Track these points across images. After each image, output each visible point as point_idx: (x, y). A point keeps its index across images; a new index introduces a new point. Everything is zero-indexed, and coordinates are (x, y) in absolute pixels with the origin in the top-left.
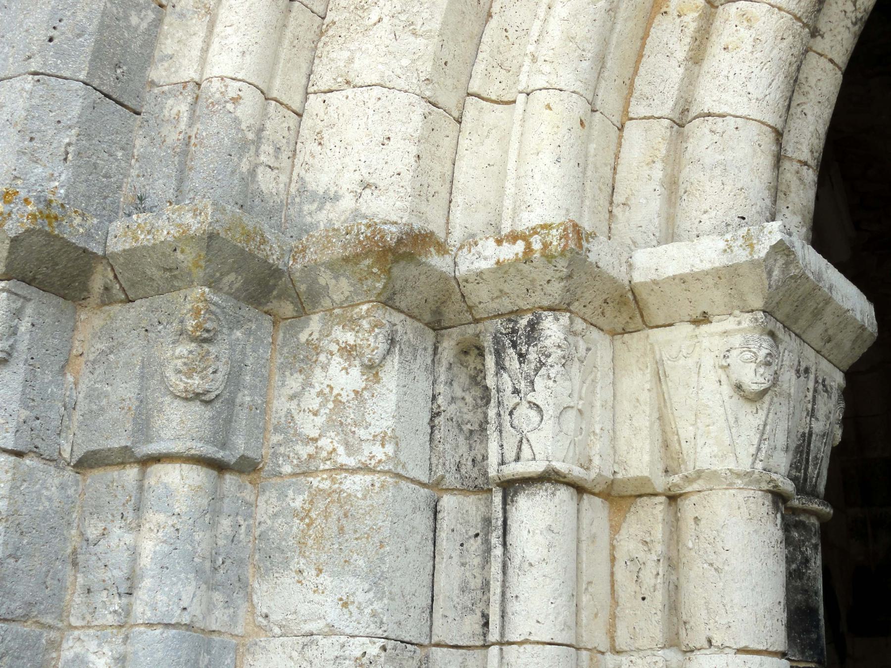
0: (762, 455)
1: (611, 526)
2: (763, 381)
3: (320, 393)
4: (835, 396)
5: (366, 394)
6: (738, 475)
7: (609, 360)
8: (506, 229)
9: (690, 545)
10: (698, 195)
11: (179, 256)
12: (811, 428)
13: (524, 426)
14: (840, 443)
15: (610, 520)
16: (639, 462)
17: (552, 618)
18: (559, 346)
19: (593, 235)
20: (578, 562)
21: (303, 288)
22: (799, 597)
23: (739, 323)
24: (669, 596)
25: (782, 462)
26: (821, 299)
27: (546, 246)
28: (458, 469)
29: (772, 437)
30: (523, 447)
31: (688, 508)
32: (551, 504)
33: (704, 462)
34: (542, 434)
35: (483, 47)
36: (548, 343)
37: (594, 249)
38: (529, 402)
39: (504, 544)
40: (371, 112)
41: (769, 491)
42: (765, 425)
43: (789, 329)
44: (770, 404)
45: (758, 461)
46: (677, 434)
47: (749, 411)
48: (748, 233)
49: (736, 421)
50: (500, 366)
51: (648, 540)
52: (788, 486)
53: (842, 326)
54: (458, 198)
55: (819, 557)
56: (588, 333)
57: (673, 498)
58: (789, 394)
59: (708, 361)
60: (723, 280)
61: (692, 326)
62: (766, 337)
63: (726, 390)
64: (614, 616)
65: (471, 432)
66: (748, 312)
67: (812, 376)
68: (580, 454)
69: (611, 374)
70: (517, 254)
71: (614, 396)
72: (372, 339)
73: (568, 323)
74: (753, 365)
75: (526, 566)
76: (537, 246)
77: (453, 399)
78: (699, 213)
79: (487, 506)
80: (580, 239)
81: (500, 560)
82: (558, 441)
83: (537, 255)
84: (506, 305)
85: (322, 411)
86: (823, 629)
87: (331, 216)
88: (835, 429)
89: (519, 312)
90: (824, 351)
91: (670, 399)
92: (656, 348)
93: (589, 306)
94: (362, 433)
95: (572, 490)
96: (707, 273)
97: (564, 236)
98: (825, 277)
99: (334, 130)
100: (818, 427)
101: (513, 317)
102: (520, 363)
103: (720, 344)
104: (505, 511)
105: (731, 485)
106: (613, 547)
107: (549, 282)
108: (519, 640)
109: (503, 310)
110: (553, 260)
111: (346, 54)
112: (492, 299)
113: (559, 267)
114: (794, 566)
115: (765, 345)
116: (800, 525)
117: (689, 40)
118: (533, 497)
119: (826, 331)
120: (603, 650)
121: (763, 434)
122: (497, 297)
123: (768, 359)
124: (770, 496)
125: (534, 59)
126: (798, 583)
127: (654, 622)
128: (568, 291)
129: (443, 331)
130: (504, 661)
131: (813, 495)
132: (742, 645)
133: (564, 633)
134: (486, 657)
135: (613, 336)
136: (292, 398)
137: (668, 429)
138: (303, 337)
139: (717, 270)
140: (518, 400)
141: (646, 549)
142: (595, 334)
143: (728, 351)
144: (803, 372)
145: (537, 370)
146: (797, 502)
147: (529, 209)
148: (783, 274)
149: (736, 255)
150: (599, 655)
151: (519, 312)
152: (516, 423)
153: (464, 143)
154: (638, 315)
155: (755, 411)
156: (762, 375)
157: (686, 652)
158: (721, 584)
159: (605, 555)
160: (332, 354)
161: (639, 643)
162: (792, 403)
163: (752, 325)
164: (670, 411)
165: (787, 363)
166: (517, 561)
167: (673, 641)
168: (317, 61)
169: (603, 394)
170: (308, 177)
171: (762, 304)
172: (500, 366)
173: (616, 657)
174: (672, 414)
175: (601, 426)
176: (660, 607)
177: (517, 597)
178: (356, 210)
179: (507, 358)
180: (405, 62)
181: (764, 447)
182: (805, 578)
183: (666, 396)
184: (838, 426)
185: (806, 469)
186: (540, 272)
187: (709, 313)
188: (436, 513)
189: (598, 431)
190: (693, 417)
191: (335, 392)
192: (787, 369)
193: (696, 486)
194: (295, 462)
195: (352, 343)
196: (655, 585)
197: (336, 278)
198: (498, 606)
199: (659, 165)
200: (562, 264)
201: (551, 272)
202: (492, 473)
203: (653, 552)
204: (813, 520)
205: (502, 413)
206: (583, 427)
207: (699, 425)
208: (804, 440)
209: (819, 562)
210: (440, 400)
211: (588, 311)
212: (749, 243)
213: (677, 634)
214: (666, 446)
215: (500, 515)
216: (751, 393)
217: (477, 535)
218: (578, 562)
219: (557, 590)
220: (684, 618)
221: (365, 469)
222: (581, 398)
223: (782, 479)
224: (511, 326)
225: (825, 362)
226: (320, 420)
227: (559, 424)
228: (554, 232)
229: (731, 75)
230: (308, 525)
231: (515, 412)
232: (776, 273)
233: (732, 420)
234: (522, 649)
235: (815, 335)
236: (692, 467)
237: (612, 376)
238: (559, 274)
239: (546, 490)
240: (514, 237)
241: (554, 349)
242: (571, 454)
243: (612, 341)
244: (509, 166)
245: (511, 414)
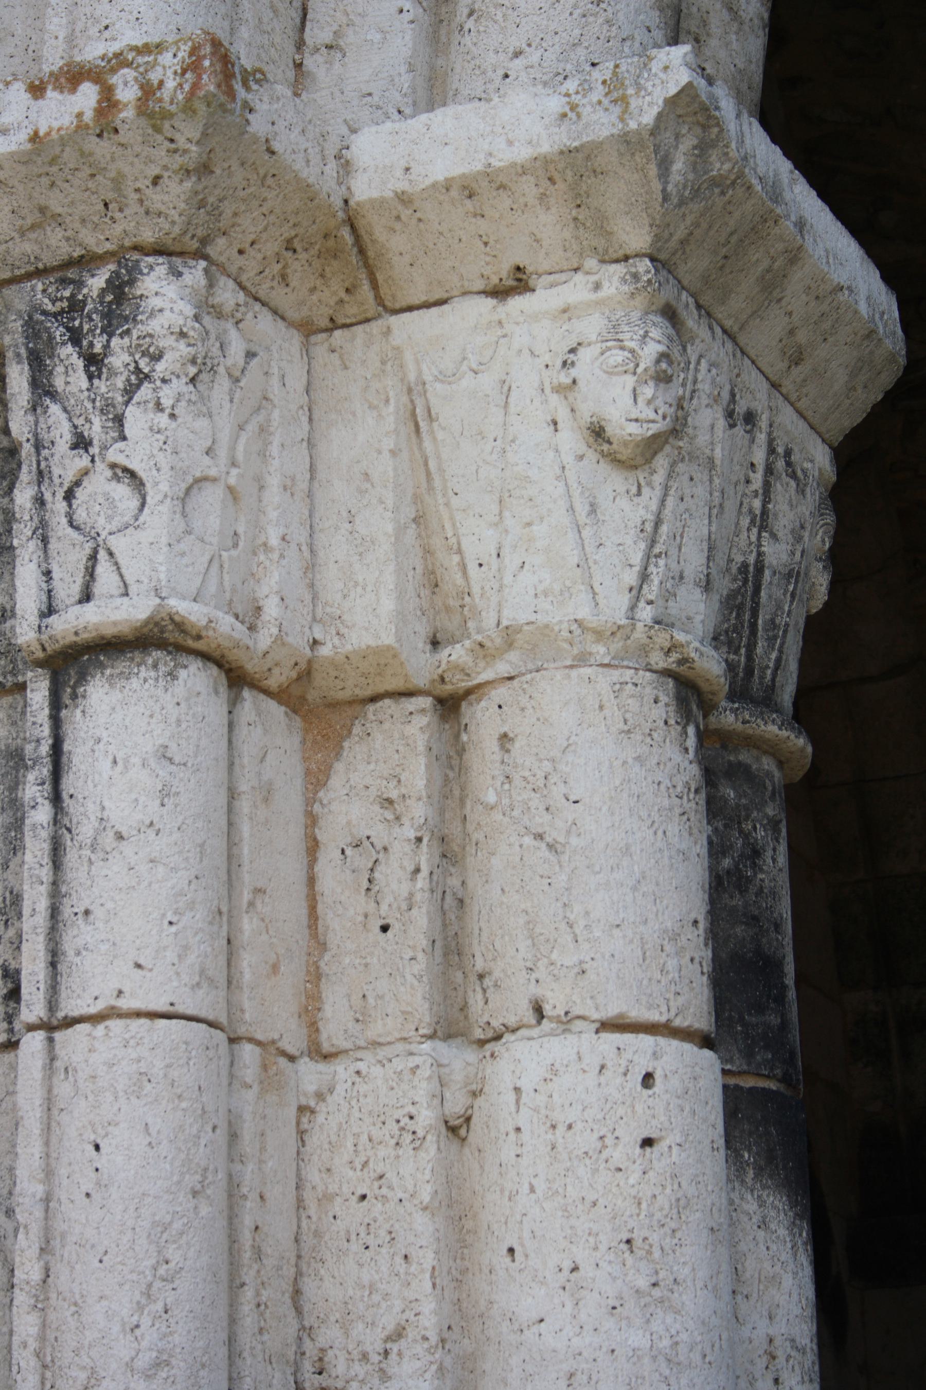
0: (652, 591)
1: (308, 772)
2: (652, 416)
4: (813, 496)
6: (599, 635)
7: (300, 385)
8: (53, 59)
9: (491, 798)
10: (499, 17)
12: (760, 554)
13: (101, 521)
14: (826, 604)
15: (305, 759)
16: (369, 615)
17: (171, 955)
18: (182, 335)
19: (255, 77)
22: (739, 930)
23: (597, 286)
24: (445, 925)
25: (697, 611)
26: (780, 246)
27: (148, 91)
29: (673, 552)
30: (99, 569)
31: (483, 719)
32: (168, 699)
33: (519, 607)
34: (145, 536)
36: (155, 325)
37: (262, 107)
38: (113, 466)
39: (56, 799)
41: (667, 673)
42: (658, 523)
43: (709, 315)
44: (669, 476)
45: (642, 604)
46: (459, 551)
47: (622, 489)
48: (615, 73)
49: (593, 509)
50: (43, 389)
51: (394, 794)
52: (711, 665)
53: (827, 325)
55: (783, 848)
56: (250, 315)
57: (450, 705)
58: (711, 460)
59: (527, 377)
60: (561, 185)
61: (491, 302)
62: (658, 319)
63: (570, 440)
64: (315, 976)
66: (617, 261)
67: (762, 437)
68: (234, 590)
69: (305, 419)
70: (79, 115)
71: (312, 469)
73: (204, 282)
74: (630, 380)
75: (108, 839)
76: (127, 92)
78: (502, 56)
79: (14, 723)
80: (228, 76)
81: (44, 834)
82: (183, 554)
83: (128, 114)
84: (56, 245)
86: (795, 1008)
88: (813, 572)
89: (87, 262)
90: (788, 386)
91: (441, 470)
92: (408, 357)
93: (251, 252)
95: (215, 670)
96: (523, 170)
97: (193, 66)
98: (787, 195)
100: (776, 554)
101: (71, 274)
102: (90, 377)
103: (551, 339)
104: (56, 722)
105: (582, 660)
106: (312, 820)
107: (156, 180)
108: (93, 1010)
109: (48, 259)
110: (167, 125)
112: (22, 233)
113: (181, 142)
114: (727, 863)
115: (655, 333)
116: (740, 773)
118: (123, 682)
119: (792, 332)
120: (291, 1050)
121: (653, 542)
122: (33, 227)
123: (664, 366)
124: (671, 683)
126: (737, 901)
127: (409, 977)
128: (202, 205)
130: (58, 1064)
131: (767, 706)
132: (611, 1011)
133: (201, 993)
134: (13, 1067)
135: (307, 336)
137: (437, 542)
139: (545, 161)
140: (85, 461)
141: (390, 817)
142: (264, 324)
143: (573, 351)
145: (130, 392)
146: (731, 718)
147: (107, 34)
148: (694, 170)
149: (587, 125)
150: (282, 1061)
151: (87, 262)
152: (81, 515)
154: (366, 287)
155: (634, 490)
156: (649, 402)
157: (482, 1043)
158: (564, 877)
159: (291, 836)
161: (376, 1030)
162: (717, 481)
163: (626, 288)
164: (441, 501)
165: (705, 387)
166: (86, 831)
167: (451, 1026)
169: (285, 461)
171: (649, 239)
172: (43, 389)
173: (322, 1066)
174: (447, 504)
175: (282, 531)
176: (424, 943)
177: (87, 912)
179: (60, 369)
181: (657, 572)
182: (753, 889)
183: (432, 464)
184: (820, 565)
185: (751, 647)
186: (136, 158)
187: (530, 269)
189: (274, 541)
190: (495, 508)
192: (705, 401)
193: (502, 668)
196: (411, 895)
198: (41, 938)
200: (188, 132)
201: (160, 153)
202: (25, 633)
203: (405, 820)
204: (768, 764)
205: (48, 496)
206: (241, 530)
207: (509, 522)
208: (745, 581)
209: (782, 860)
211: (250, 265)
212: (617, 94)
213: (464, 1008)
214: (433, 582)
215: (46, 731)
216: (625, 444)
219: (181, 894)
220: (480, 965)
222: (234, 464)
223: (696, 644)
224: (67, 293)
225: (789, 410)
227: (184, 515)
228: (166, 58)
231: (80, 493)
232: (679, 165)
233: (582, 509)
234: (100, 1030)
235: (765, 337)
236: (493, 622)
237: (306, 427)
238: (178, 160)
239: (155, 666)
240: (73, 76)
241: (170, 341)
242: (212, 588)
243: (306, 348)
245: (69, 496)
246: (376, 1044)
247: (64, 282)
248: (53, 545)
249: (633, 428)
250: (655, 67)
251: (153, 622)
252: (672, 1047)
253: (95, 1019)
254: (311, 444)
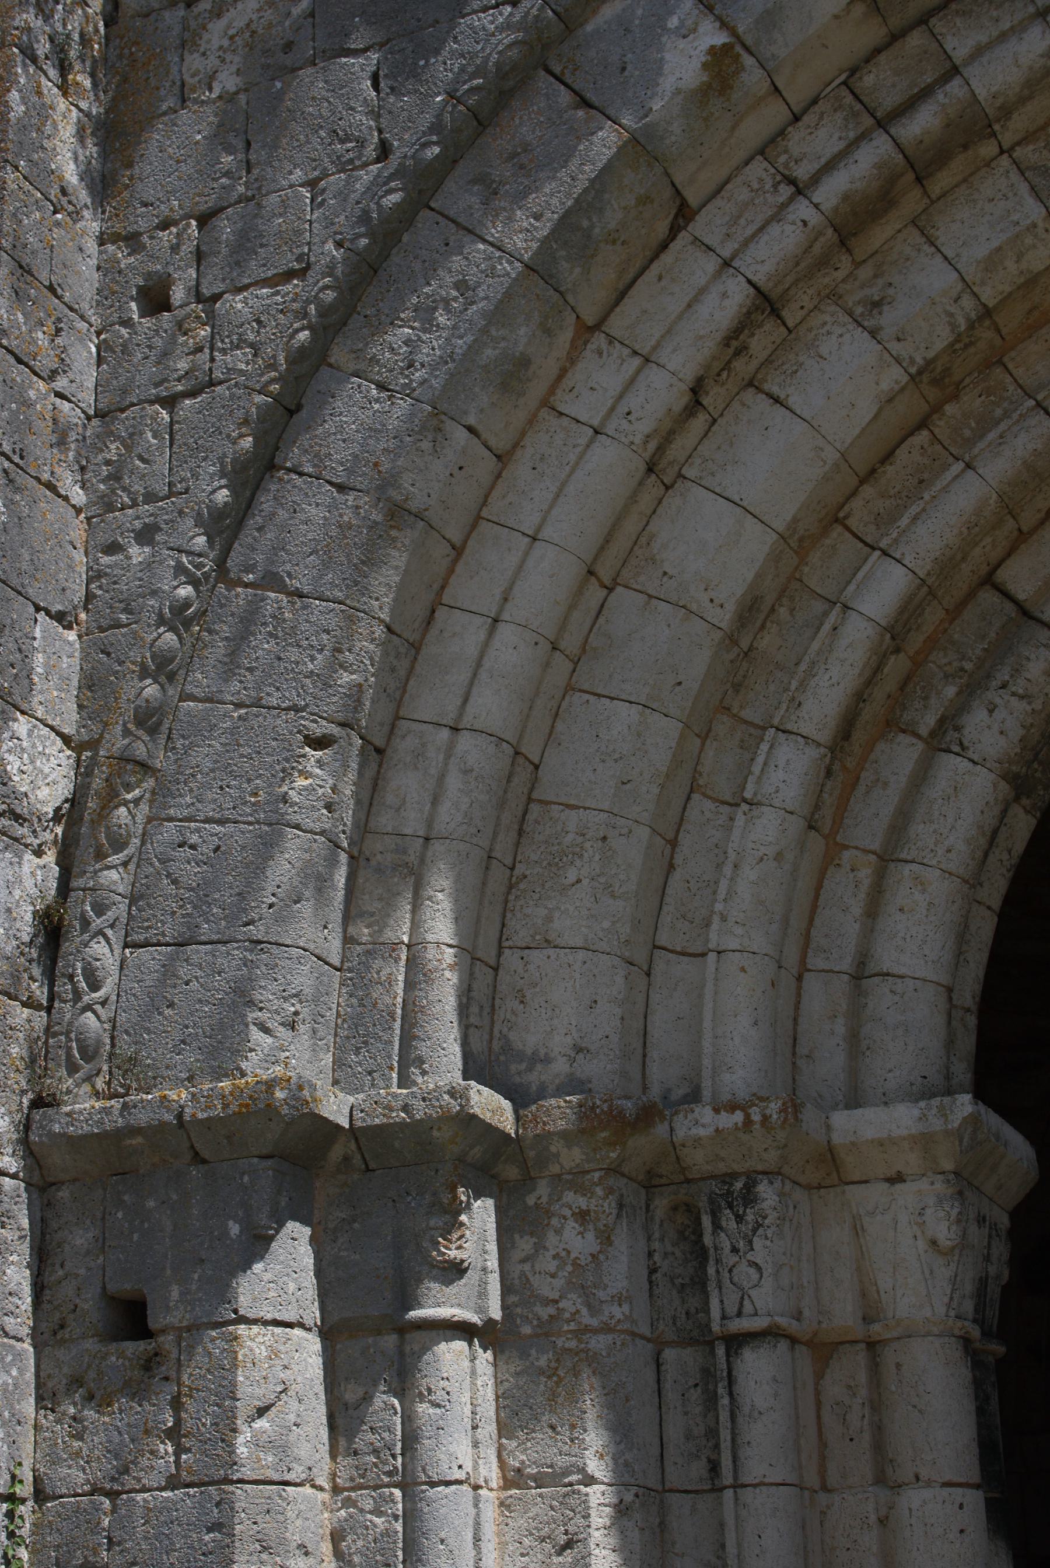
0: (954, 1304)
3: (554, 1257)
5: (602, 1257)
9: (893, 1388)
11: (435, 1133)
16: (844, 1314)
20: (796, 1408)
21: (532, 1154)
27: (765, 1118)
28: (674, 1323)
35: (667, 899)
36: (765, 1205)
39: (731, 1394)
40: (577, 976)
50: (717, 1226)
52: (976, 1332)
54: (654, 1054)
63: (921, 1244)
65: (683, 1285)
71: (815, 1248)
72: (606, 1205)
74: (947, 1223)
75: (756, 1414)
77: (666, 1255)
84: (722, 1168)
85: (560, 1274)
87: (543, 1078)
94: (601, 1294)
99: (537, 990)
100: (992, 1270)
101: (727, 1180)
111: (542, 912)
117: (863, 896)
125: (724, 919)
129: (656, 1190)
132: (946, 1479)
136: (523, 1261)
138: (531, 1200)
144: (981, 1220)
145: (754, 1231)
151: (734, 1176)
152: (736, 1279)
153: (655, 997)
157: (892, 1488)
160: (565, 1218)
166: (746, 1410)
167: (880, 1480)
168: (509, 915)
170: (513, 1036)
172: (717, 1226)
178: (572, 1074)
180: (606, 924)
188: (658, 1365)
191: (573, 1256)
194: (535, 1322)
195: (584, 1208)
197: (569, 1148)
199: (841, 1020)
202: (716, 1328)
210: (657, 1257)
217: (696, 1385)
218: (796, 1408)
221: (606, 1329)
226: (559, 1283)
228: (772, 1105)
229: (908, 936)
230: (556, 1383)
234: (758, 1490)
244: (705, 1025)
245: (730, 1271)
246: (850, 1487)
247: (724, 1182)
248: (724, 1290)
249: (948, 1243)
250: (958, 1103)
251: (770, 1327)
252: (969, 1492)
253: (755, 1486)
254: (813, 1237)
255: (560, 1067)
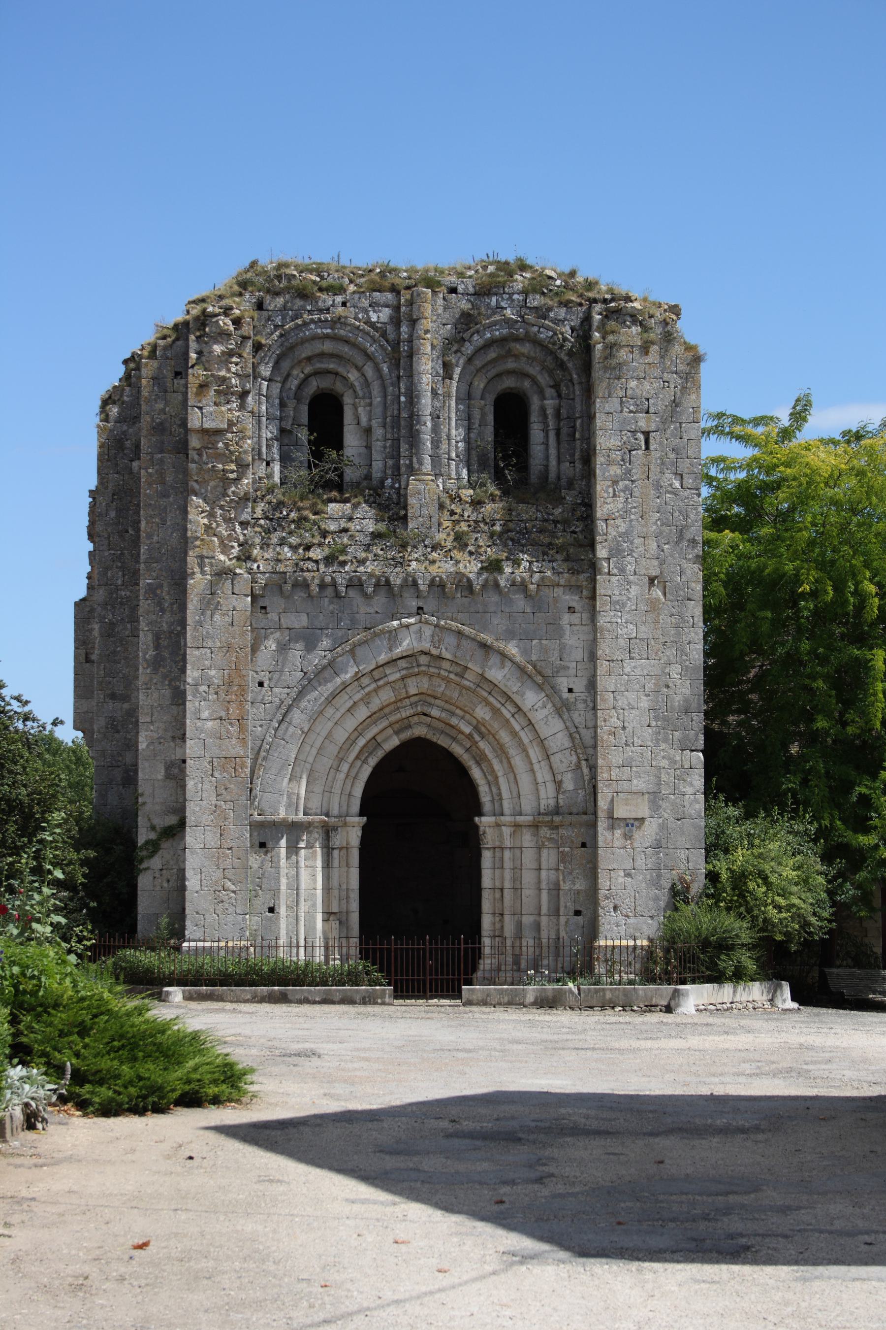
255: (314, 810)
